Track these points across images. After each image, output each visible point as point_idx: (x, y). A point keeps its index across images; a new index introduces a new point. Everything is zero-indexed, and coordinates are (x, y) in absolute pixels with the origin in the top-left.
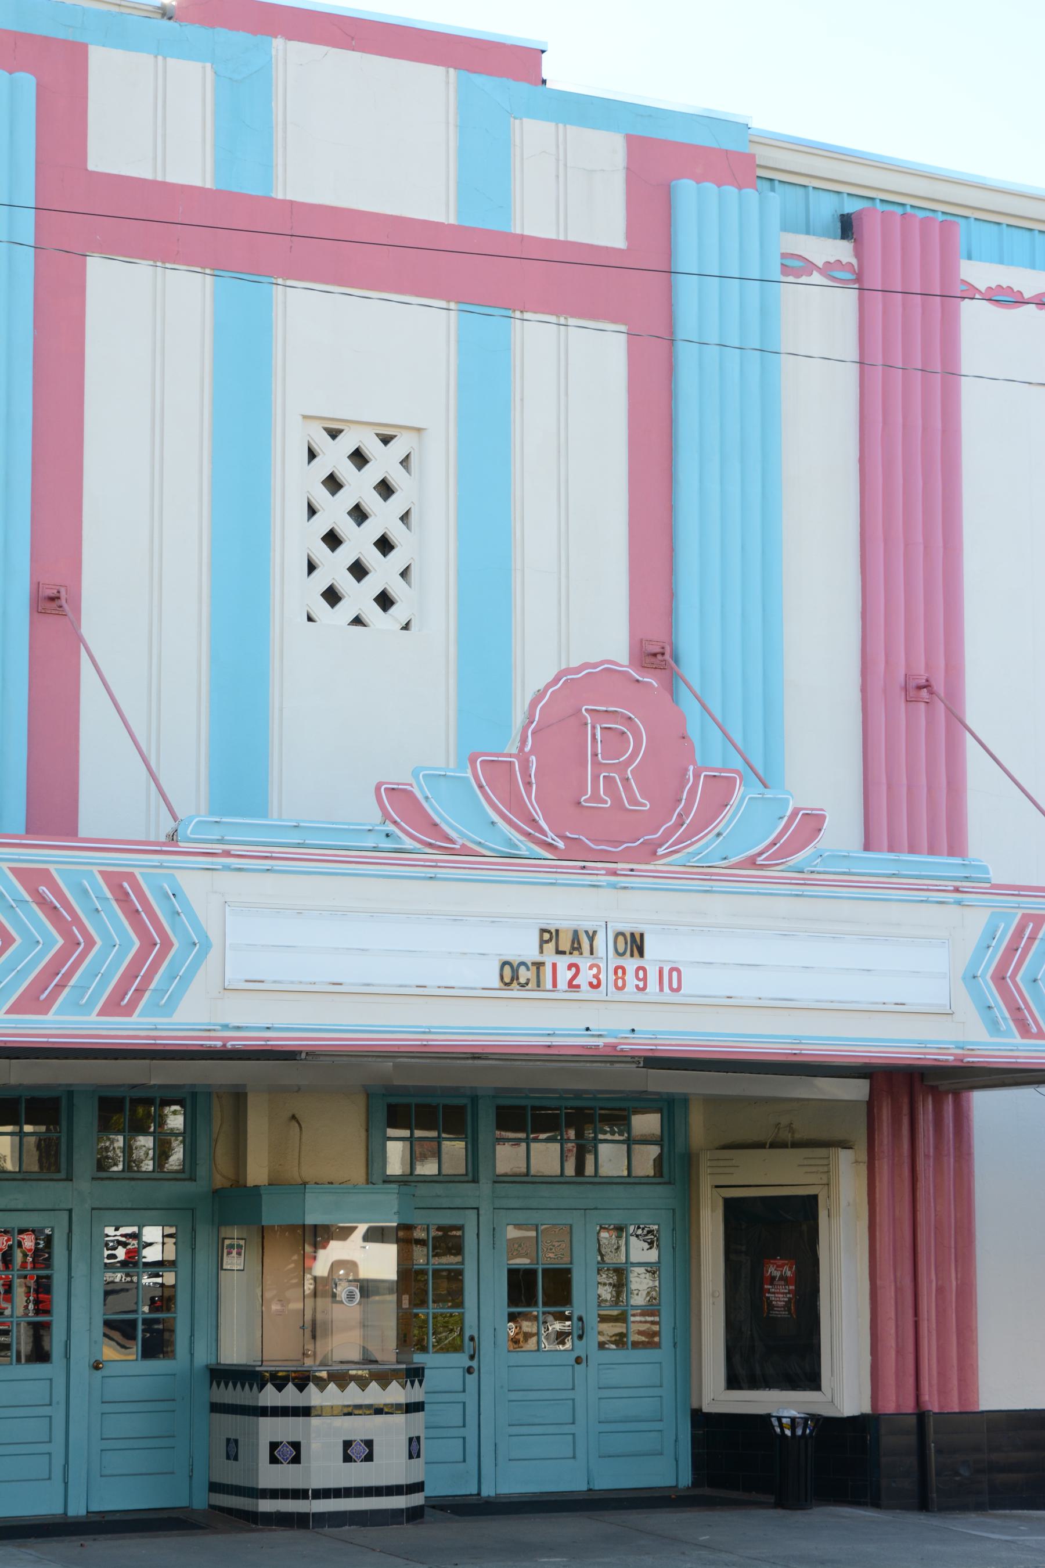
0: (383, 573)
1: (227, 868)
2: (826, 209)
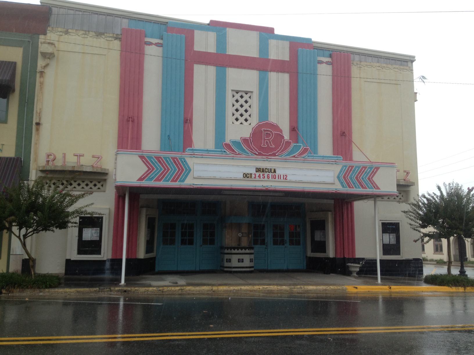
0: (246, 115)
1: (194, 157)
2: (327, 53)
